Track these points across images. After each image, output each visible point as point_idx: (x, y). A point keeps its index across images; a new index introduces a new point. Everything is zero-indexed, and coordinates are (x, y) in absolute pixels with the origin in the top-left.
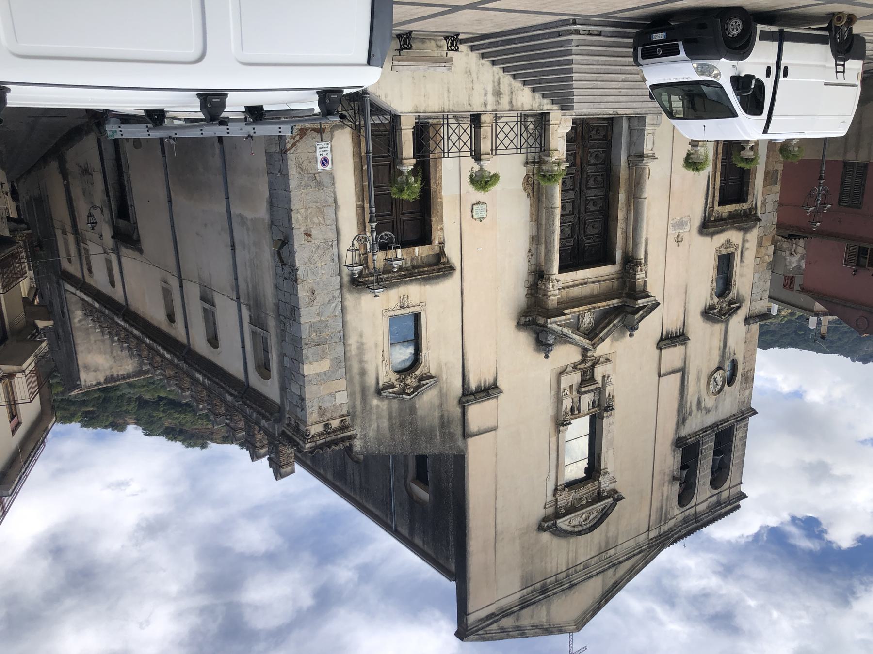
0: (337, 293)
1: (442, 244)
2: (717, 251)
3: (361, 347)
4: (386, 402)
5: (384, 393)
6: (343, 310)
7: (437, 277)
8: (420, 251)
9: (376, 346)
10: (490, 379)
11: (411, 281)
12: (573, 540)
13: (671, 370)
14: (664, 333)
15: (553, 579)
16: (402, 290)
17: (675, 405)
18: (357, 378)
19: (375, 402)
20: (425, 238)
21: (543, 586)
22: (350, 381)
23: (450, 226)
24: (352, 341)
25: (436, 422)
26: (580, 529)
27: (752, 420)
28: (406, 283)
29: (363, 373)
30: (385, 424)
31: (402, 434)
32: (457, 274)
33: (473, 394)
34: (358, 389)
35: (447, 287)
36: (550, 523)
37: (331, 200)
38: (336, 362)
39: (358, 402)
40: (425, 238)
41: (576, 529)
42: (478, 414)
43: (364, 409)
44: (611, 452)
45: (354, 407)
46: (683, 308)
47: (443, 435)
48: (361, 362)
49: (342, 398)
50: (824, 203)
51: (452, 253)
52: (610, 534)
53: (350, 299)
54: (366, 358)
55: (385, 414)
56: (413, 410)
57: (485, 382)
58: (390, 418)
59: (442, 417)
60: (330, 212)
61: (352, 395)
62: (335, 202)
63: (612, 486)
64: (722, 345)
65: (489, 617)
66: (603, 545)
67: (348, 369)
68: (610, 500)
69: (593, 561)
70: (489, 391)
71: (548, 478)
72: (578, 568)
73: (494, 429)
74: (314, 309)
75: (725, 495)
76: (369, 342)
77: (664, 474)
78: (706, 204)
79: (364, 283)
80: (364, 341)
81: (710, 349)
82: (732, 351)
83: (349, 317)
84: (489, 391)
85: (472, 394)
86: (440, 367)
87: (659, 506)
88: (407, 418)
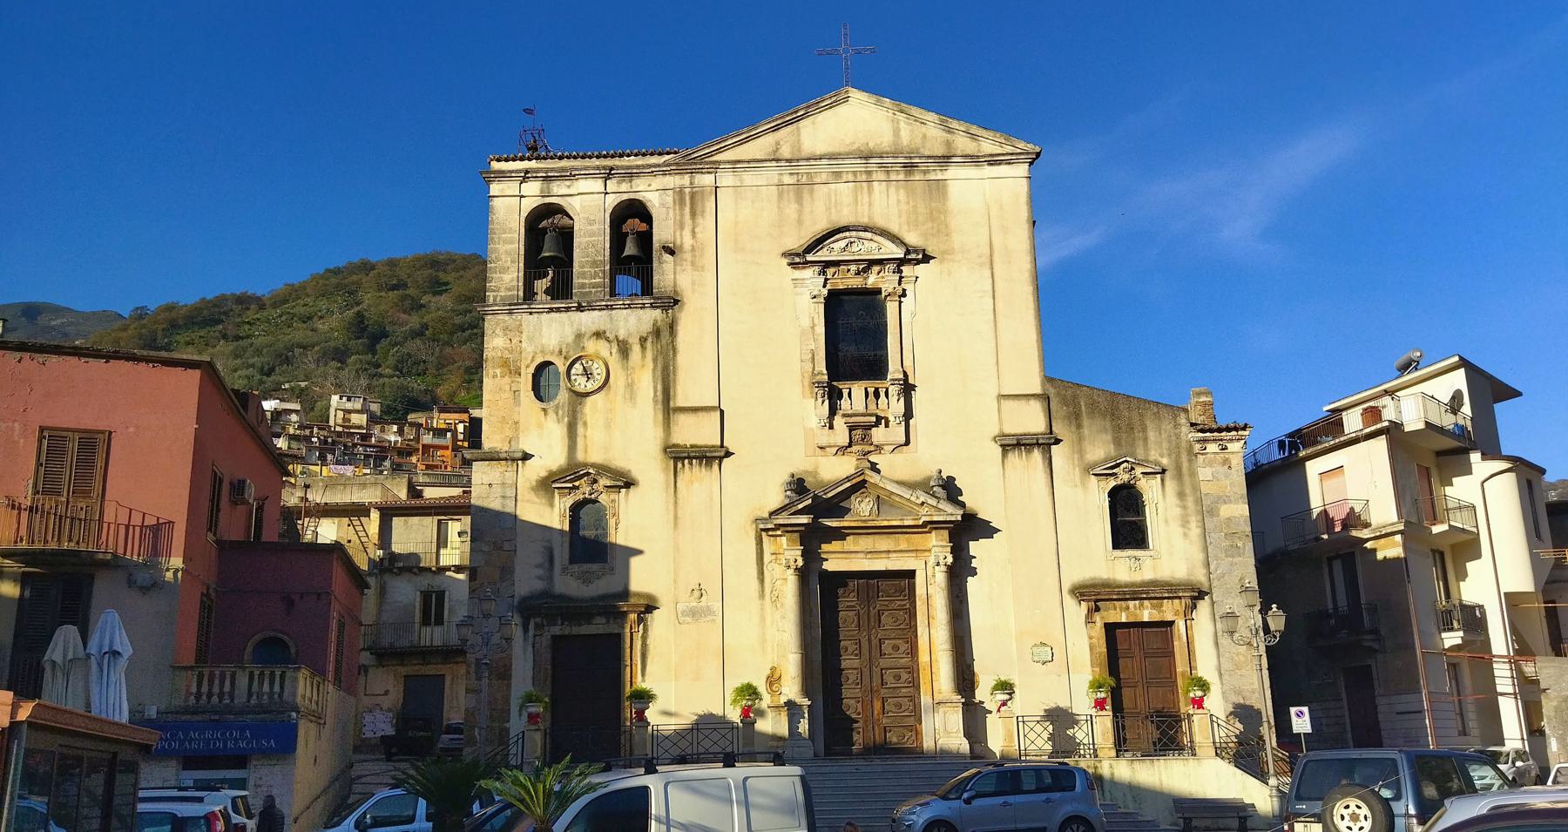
0: (1215, 583)
1: (1089, 620)
2: (612, 569)
3: (1185, 523)
4: (1152, 458)
5: (1158, 469)
6: (1208, 565)
7: (1094, 586)
8: (1119, 614)
9: (1166, 521)
10: (1013, 457)
11: (1126, 586)
12: (864, 220)
13: (700, 414)
14: (716, 467)
15: (893, 177)
16: (1138, 577)
17: (682, 359)
18: (1188, 490)
19: (1165, 461)
20: (1110, 628)
21: (908, 173)
22: (1196, 488)
23: (1081, 644)
24: (1195, 531)
25: (1086, 422)
26: (862, 234)
27: (656, 612)
28: (1133, 585)
29: (1181, 495)
30: (1151, 435)
31: (1130, 418)
32: (1066, 586)
33: (1038, 445)
34: (1186, 479)
35: (1076, 573)
36: (913, 256)
37: (1226, 677)
38: (1213, 512)
39: (1185, 465)
40: (1110, 628)
41: (868, 235)
42: (1031, 420)
43: (1178, 455)
44: (806, 323)
45: (1190, 461)
46: (680, 495)
47: (1077, 405)
48: (1184, 507)
49: (1204, 473)
50: (381, 376)
51: (1077, 611)
52: (794, 206)
53: (1200, 576)
54: (1178, 511)
55: (1151, 445)
56: (1117, 442)
57: (1020, 455)
58: (1146, 439)
59: (1079, 426)
60: (1226, 665)
61: (1193, 474)
62: (1221, 675)
63: (798, 274)
64: (580, 430)
65: (999, 163)
66: (806, 196)
67: (1199, 501)
68: (810, 258)
69: (824, 177)
70: (1014, 444)
71: (914, 315)
72: (851, 177)
73: (1003, 397)
74: (1237, 573)
75: (532, 188)
76: (1176, 529)
77: (693, 264)
78: (644, 638)
79: (1193, 590)
80: (1181, 530)
81: (608, 425)
82: (550, 412)
83: (1201, 556)
84: (1014, 444)
85: (1045, 443)
86: (1084, 484)
87: (699, 220)
88: (1124, 436)
